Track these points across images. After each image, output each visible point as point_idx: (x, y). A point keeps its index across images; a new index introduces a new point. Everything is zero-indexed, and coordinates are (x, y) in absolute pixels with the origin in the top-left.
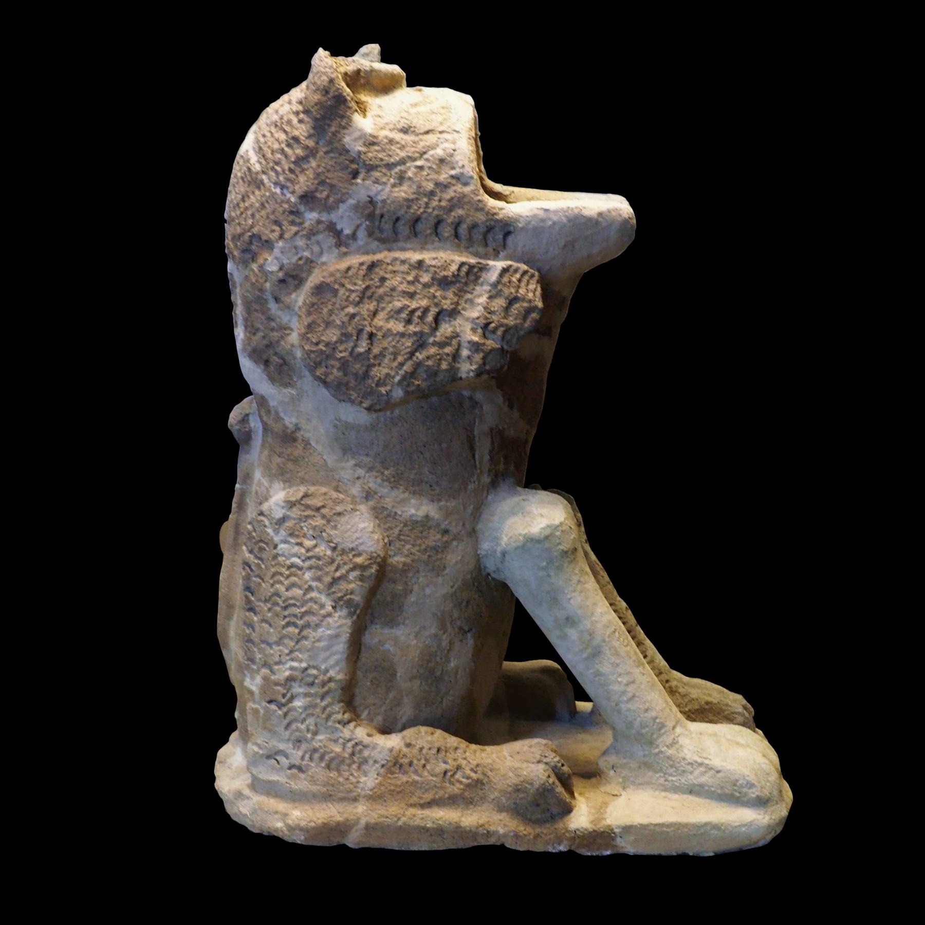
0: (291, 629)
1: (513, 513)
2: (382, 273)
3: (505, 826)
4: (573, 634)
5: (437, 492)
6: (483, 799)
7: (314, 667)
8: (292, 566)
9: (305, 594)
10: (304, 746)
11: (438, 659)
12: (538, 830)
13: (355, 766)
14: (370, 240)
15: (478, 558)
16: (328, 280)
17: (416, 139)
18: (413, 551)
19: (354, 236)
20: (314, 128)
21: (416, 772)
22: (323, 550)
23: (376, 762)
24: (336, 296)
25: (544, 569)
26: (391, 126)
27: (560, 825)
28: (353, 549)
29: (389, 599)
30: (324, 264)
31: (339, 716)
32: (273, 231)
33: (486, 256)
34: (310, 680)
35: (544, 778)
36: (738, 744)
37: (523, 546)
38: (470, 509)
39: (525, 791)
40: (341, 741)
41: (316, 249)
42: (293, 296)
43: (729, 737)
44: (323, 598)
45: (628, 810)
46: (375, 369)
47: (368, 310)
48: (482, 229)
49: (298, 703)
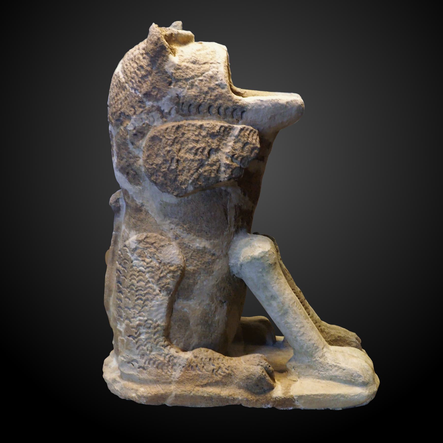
0: (139, 301)
1: (246, 246)
2: (183, 131)
3: (242, 395)
5: (209, 235)
6: (231, 383)
7: (150, 320)
8: (140, 271)
9: (146, 285)
10: (146, 357)
11: (210, 316)
12: (258, 398)
13: (170, 367)
14: (177, 115)
15: (229, 267)
16: (157, 134)
17: (199, 66)
18: (198, 264)
19: (169, 113)
20: (150, 61)
21: (199, 370)
22: (155, 263)
23: (180, 365)
24: (161, 142)
25: (261, 272)
26: (187, 61)
27: (268, 395)
28: (169, 263)
29: (186, 287)
30: (155, 126)
31: (163, 343)
32: (131, 111)
33: (233, 123)
34: (148, 325)
35: (261, 373)
36: (353, 356)
37: (251, 261)
38: (225, 244)
39: (251, 379)
40: (163, 355)
41: (151, 119)
42: (141, 142)
43: (349, 353)
44: (155, 287)
45: (301, 388)
46: (180, 177)
47: (176, 148)
48: (231, 110)
49: (143, 337)
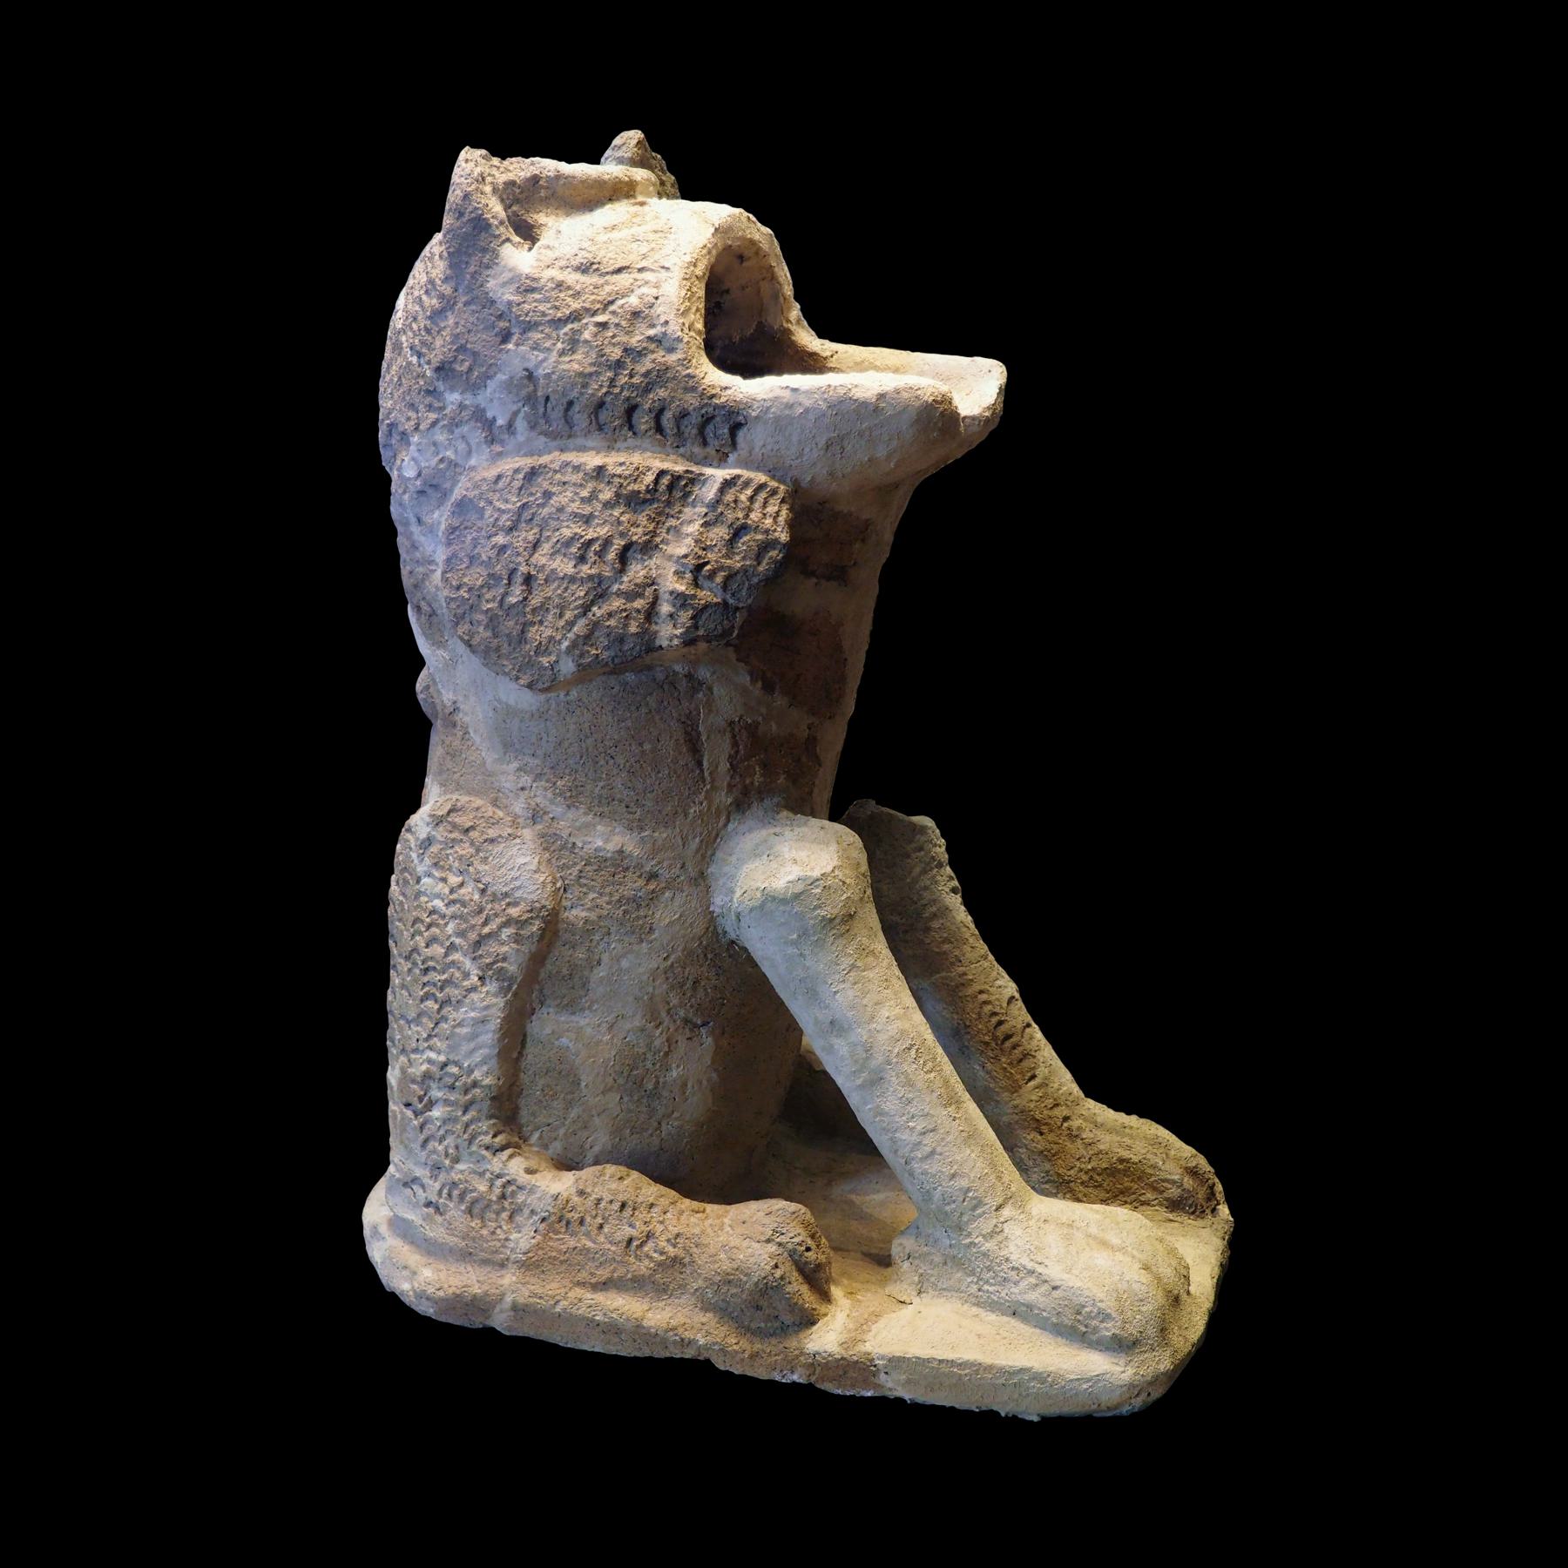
0: (430, 1003)
1: (755, 854)
2: (545, 485)
3: (708, 1333)
4: (841, 1046)
5: (637, 816)
6: (682, 1287)
7: (456, 1063)
8: (433, 912)
9: (446, 955)
10: (442, 1177)
11: (649, 1064)
12: (758, 1346)
13: (505, 1215)
14: (534, 434)
15: (712, 920)
16: (471, 494)
17: (601, 281)
18: (602, 901)
19: (510, 426)
20: (451, 266)
21: (587, 1234)
22: (469, 892)
23: (533, 1212)
24: (482, 518)
25: (794, 943)
26: (563, 263)
27: (792, 1343)
28: (506, 895)
29: (565, 971)
30: (473, 468)
31: (487, 1139)
32: (409, 419)
33: (705, 461)
34: (450, 1081)
35: (768, 1268)
36: (1104, 1244)
37: (762, 906)
38: (694, 844)
39: (740, 1284)
40: (488, 1175)
41: (462, 446)
42: (436, 515)
43: (1093, 1230)
44: (468, 964)
45: (905, 1331)
46: (533, 629)
47: (525, 539)
48: (695, 419)
49: (436, 1113)
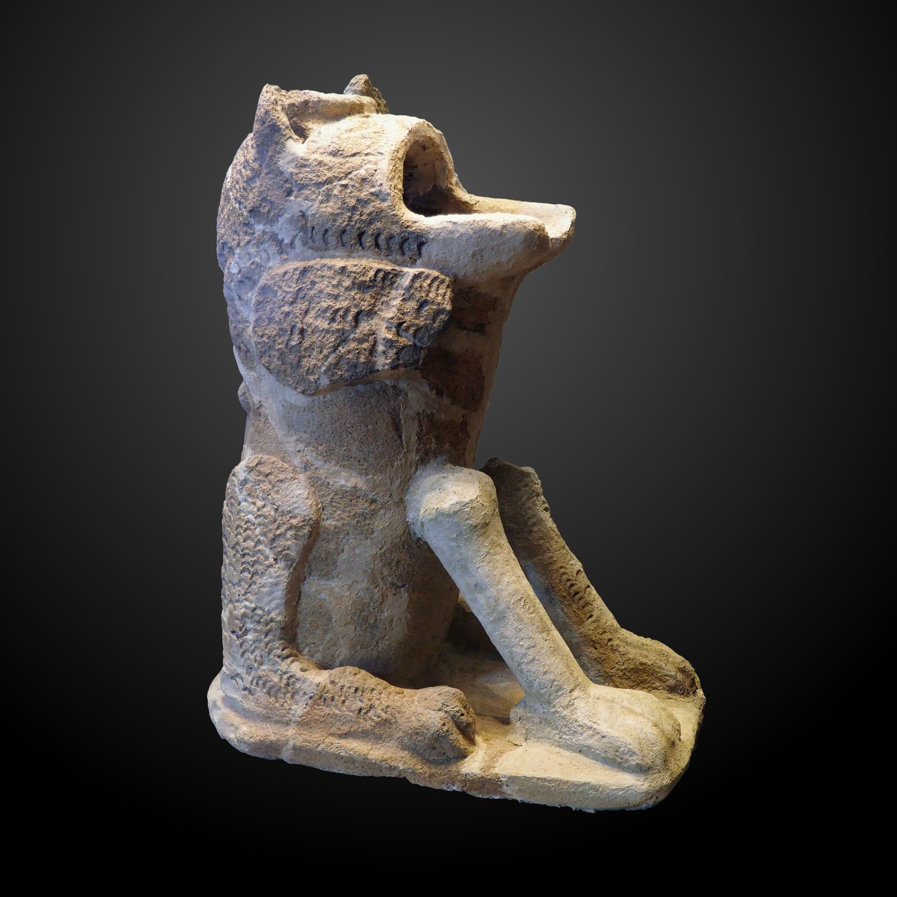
0: (246, 574)
1: (432, 489)
2: (312, 277)
3: (405, 763)
4: (481, 598)
5: (364, 467)
6: (390, 736)
7: (261, 608)
8: (248, 522)
9: (255, 546)
10: (253, 673)
11: (371, 609)
12: (433, 770)
13: (289, 695)
14: (305, 248)
15: (407, 526)
16: (269, 283)
17: (344, 161)
18: (344, 515)
19: (292, 244)
20: (258, 152)
21: (336, 706)
22: (269, 510)
23: (305, 693)
24: (276, 296)
25: (454, 540)
26: (322, 150)
27: (453, 768)
28: (290, 512)
29: (323, 556)
30: (270, 268)
31: (279, 652)
32: (234, 240)
33: (403, 264)
34: (257, 618)
35: (439, 725)
36: (632, 712)
37: (436, 518)
38: (397, 483)
39: (423, 735)
40: (279, 672)
41: (264, 255)
42: (249, 295)
43: (625, 704)
44: (268, 551)
45: (518, 761)
46: (305, 360)
47: (300, 309)
48: (398, 240)
49: (250, 637)
